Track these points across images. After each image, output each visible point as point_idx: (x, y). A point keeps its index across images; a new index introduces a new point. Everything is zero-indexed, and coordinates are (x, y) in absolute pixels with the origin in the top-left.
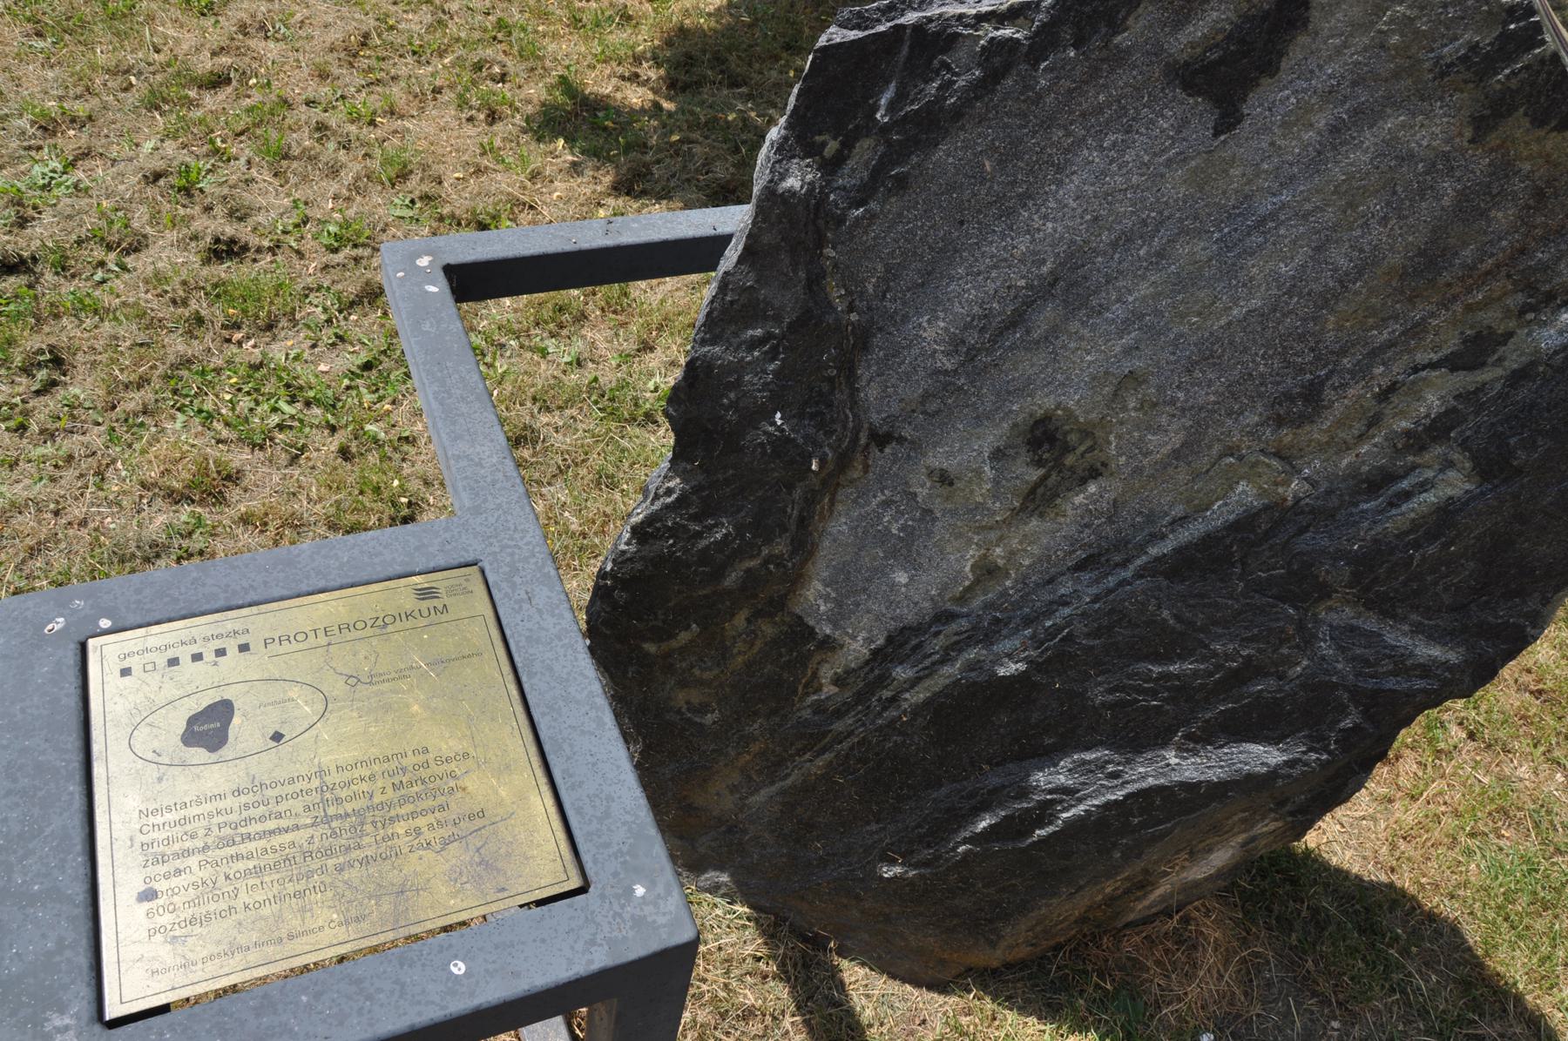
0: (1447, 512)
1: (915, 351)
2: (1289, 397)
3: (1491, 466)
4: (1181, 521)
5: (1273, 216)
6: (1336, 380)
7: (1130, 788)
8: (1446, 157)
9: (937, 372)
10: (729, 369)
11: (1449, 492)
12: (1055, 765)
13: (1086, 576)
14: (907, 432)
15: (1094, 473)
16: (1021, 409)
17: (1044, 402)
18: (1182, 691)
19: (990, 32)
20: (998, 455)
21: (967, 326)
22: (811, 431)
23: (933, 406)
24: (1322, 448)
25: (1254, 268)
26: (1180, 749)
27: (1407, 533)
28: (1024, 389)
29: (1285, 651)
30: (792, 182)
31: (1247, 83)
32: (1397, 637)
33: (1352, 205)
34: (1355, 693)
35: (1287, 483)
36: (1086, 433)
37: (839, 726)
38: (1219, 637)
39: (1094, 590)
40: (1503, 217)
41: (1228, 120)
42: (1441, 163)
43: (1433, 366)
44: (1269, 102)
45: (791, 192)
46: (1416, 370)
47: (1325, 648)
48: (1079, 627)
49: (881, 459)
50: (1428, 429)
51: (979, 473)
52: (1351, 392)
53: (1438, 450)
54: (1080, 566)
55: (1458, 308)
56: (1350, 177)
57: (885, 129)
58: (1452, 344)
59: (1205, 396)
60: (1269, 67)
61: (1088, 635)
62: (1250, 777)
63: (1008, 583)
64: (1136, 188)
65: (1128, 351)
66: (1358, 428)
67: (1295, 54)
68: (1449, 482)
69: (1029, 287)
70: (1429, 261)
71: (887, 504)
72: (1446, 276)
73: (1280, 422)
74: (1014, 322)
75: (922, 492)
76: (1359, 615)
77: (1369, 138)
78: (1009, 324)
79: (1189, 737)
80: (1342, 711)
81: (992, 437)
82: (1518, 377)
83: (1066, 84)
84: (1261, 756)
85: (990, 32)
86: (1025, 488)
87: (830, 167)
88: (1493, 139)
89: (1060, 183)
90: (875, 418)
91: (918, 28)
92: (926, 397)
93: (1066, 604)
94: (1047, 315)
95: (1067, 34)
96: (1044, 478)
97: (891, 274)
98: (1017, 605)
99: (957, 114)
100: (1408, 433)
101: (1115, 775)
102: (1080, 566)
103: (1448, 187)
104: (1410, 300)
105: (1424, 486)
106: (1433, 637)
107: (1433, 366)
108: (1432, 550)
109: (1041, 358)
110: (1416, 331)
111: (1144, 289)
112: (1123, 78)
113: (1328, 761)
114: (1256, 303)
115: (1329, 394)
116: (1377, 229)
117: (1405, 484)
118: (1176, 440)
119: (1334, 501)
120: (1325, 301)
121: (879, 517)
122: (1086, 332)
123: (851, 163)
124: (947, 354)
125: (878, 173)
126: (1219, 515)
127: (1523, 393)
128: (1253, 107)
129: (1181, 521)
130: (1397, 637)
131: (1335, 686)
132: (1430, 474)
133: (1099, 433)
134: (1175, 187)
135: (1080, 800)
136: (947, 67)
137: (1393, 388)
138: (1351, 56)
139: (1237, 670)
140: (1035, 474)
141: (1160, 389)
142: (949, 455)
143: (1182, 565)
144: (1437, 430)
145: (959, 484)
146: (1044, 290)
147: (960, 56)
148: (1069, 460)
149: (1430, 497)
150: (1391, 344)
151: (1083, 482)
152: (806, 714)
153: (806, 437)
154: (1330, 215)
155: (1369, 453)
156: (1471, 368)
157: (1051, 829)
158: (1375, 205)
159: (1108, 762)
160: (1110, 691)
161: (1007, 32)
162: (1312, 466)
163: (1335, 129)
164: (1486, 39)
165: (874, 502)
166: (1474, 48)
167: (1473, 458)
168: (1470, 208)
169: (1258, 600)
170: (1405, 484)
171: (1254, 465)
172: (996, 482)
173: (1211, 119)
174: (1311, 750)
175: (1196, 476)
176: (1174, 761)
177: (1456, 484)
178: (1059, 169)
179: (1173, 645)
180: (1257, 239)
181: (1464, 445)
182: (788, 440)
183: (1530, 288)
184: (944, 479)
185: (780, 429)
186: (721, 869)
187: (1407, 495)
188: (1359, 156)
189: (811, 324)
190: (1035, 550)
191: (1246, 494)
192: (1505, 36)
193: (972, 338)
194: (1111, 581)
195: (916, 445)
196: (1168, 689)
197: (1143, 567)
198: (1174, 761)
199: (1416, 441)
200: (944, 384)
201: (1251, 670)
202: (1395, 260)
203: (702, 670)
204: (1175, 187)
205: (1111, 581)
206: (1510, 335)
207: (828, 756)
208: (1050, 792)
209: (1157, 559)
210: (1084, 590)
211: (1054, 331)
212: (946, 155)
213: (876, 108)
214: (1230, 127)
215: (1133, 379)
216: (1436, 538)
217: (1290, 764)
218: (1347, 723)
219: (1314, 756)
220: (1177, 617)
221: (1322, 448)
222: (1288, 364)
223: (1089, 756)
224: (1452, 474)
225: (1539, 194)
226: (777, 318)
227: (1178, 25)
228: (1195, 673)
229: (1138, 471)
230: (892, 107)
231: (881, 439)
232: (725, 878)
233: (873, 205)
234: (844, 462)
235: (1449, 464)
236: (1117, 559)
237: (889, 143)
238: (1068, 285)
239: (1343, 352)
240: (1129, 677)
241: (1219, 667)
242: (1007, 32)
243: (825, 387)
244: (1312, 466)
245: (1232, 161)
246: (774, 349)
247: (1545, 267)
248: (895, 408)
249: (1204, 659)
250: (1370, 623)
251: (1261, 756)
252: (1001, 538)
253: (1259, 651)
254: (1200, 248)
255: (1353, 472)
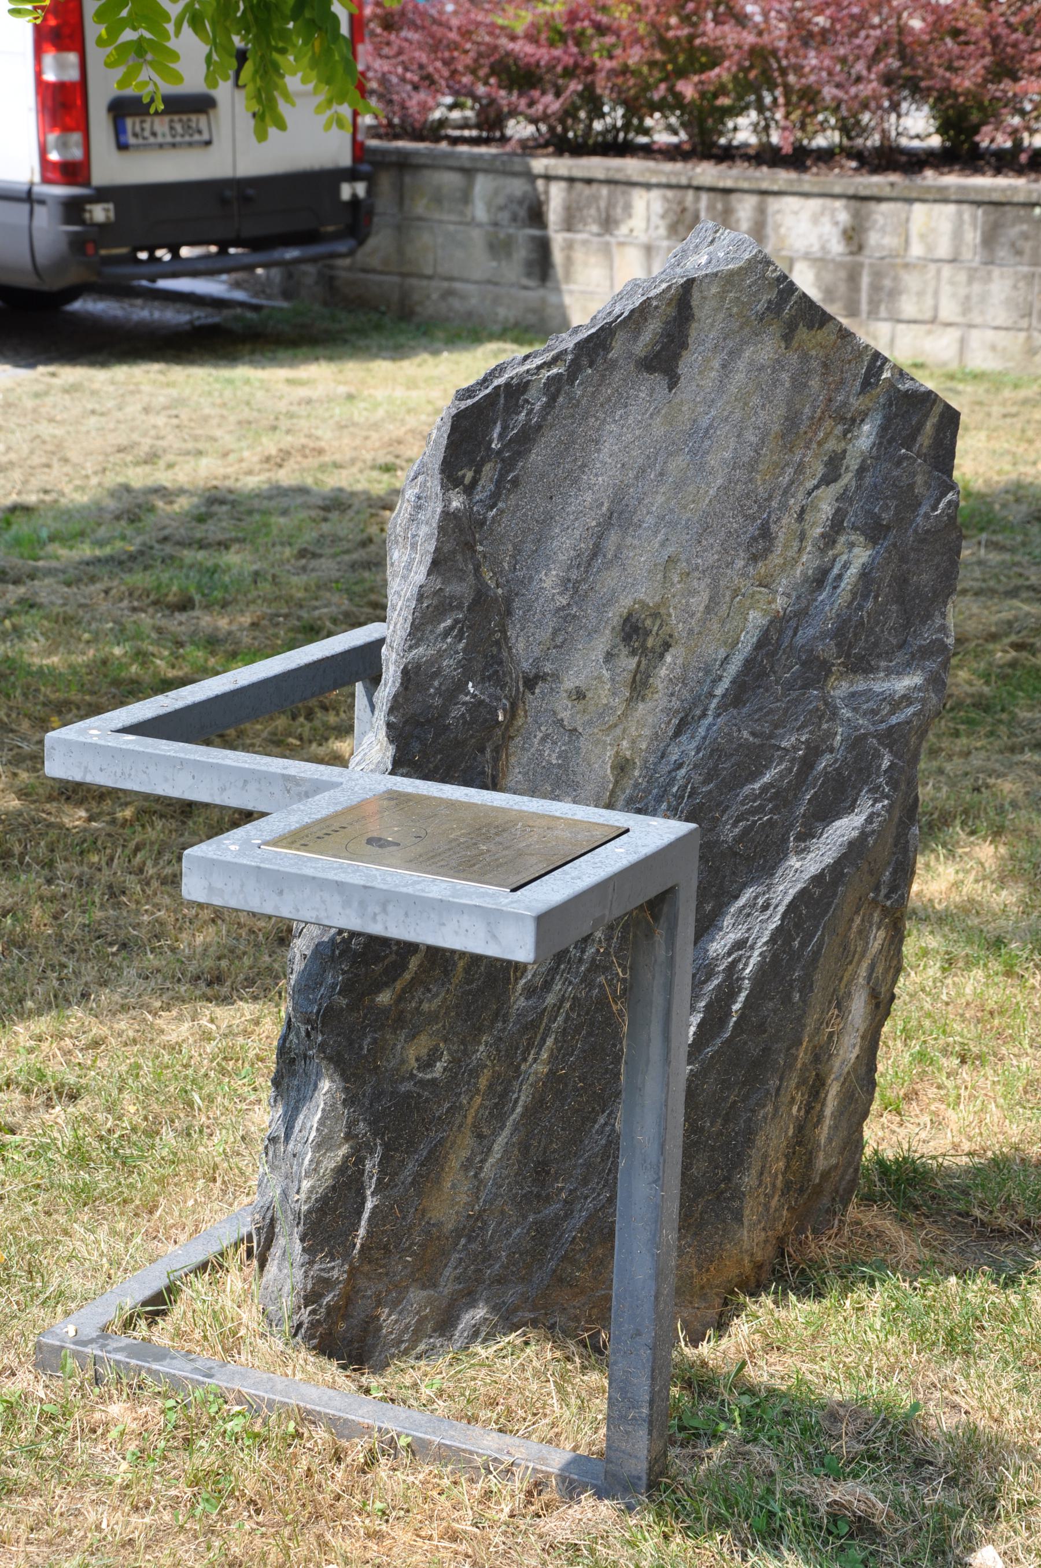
0: (865, 574)
1: (542, 600)
2: (754, 539)
3: (875, 532)
4: (726, 659)
5: (711, 426)
6: (774, 517)
7: (781, 909)
8: (778, 361)
9: (558, 610)
10: (431, 662)
11: (862, 560)
12: (721, 929)
13: (683, 738)
14: (548, 668)
15: (667, 646)
16: (614, 615)
17: (625, 603)
18: (781, 797)
19: (545, 374)
20: (609, 657)
21: (570, 568)
22: (492, 690)
23: (559, 640)
24: (783, 567)
25: (712, 461)
26: (799, 852)
27: (851, 603)
28: (611, 600)
29: (825, 726)
30: (455, 504)
31: (676, 357)
32: (880, 686)
33: (746, 404)
34: (880, 737)
35: (774, 600)
36: (655, 615)
37: (551, 999)
38: (783, 737)
39: (694, 744)
40: (815, 383)
41: (673, 382)
42: (778, 365)
43: (817, 487)
44: (689, 363)
45: (458, 509)
46: (809, 494)
47: (846, 713)
48: (697, 778)
49: (533, 701)
50: (832, 527)
51: (599, 678)
52: (784, 522)
53: (842, 539)
54: (677, 733)
55: (814, 446)
56: (740, 389)
57: (499, 452)
58: (820, 470)
59: (712, 557)
60: (684, 345)
61: (705, 783)
62: (851, 844)
63: (637, 773)
64: (638, 438)
65: (663, 545)
66: (796, 544)
67: (693, 333)
68: (857, 557)
69: (599, 525)
70: (792, 421)
71: (544, 740)
72: (803, 428)
73: (754, 558)
74: (594, 555)
75: (565, 715)
76: (852, 683)
77: (741, 365)
78: (592, 556)
79: (801, 838)
80: (878, 756)
81: (602, 643)
82: (861, 471)
83: (591, 389)
84: (845, 828)
85: (545, 374)
86: (629, 677)
87: (469, 490)
88: (795, 344)
89: (599, 451)
90: (525, 665)
91: (507, 385)
92: (555, 632)
93: (680, 766)
94: (613, 538)
95: (585, 361)
96: (639, 663)
97: (518, 550)
98: (647, 791)
99: (539, 427)
100: (823, 535)
101: (765, 907)
102: (677, 733)
103: (785, 376)
104: (791, 450)
105: (846, 566)
106: (899, 672)
107: (817, 487)
108: (869, 605)
109: (615, 572)
110: (800, 468)
111: (660, 499)
112: (618, 376)
113: (891, 806)
114: (720, 482)
115: (774, 528)
116: (762, 413)
117: (836, 571)
118: (705, 596)
119: (804, 603)
120: (752, 466)
121: (541, 753)
122: (636, 542)
123: (481, 483)
124: (561, 594)
125: (499, 483)
126: (748, 641)
127: (868, 481)
128: (682, 369)
129: (726, 659)
130: (880, 686)
131: (865, 737)
132: (845, 557)
133: (663, 611)
134: (659, 429)
135: (752, 948)
136: (527, 401)
137: (803, 511)
138: (719, 326)
139: (805, 755)
140: (633, 662)
141: (688, 561)
142: (578, 674)
143: (740, 693)
144: (836, 526)
145: (589, 695)
146: (607, 523)
147: (532, 394)
148: (650, 642)
149: (854, 570)
150: (792, 482)
151: (662, 656)
152: (522, 1002)
153: (490, 696)
154: (738, 415)
155: (808, 561)
156: (835, 480)
157: (742, 997)
158: (756, 400)
159: (756, 897)
160: (735, 825)
161: (555, 371)
162: (783, 584)
163: (724, 366)
164: (773, 295)
165: (536, 741)
166: (770, 302)
167: (863, 533)
168: (799, 385)
169: (794, 694)
170: (836, 571)
171: (753, 596)
172: (613, 680)
173: (665, 383)
174: (876, 801)
175: (723, 623)
176: (798, 865)
177: (861, 556)
178: (597, 442)
179: (755, 758)
180: (707, 443)
181: (855, 528)
182: (481, 702)
183: (842, 419)
184: (579, 695)
185: (474, 696)
186: (472, 1305)
187: (840, 577)
188: (739, 377)
189: (481, 599)
190: (647, 732)
191: (756, 619)
192: (780, 292)
193: (574, 575)
194: (702, 731)
195: (556, 677)
196: (770, 800)
197: (718, 708)
198: (798, 865)
199: (829, 539)
200: (566, 617)
201: (814, 752)
202: (776, 428)
203: (430, 1001)
204: (659, 429)
205: (702, 731)
206: (845, 451)
207: (550, 1042)
208: (729, 954)
209: (724, 696)
210: (687, 748)
211: (619, 548)
212: (537, 456)
213: (491, 442)
214: (676, 383)
215: (671, 560)
216: (868, 596)
217: (869, 820)
218: (886, 764)
219: (879, 805)
220: (753, 734)
221: (783, 567)
222: (746, 517)
223: (742, 901)
224: (856, 550)
225: (825, 365)
226: (459, 607)
227: (636, 338)
228: (782, 776)
229: (691, 631)
230: (501, 436)
231: (531, 683)
232: (480, 1312)
233: (500, 505)
234: (514, 706)
235: (852, 545)
236: (698, 712)
237: (503, 460)
238: (618, 516)
239: (770, 498)
240: (743, 803)
241: (793, 761)
242: (555, 371)
243: (495, 650)
244: (783, 584)
245: (681, 403)
246: (461, 630)
247: (845, 404)
248: (537, 652)
249: (781, 759)
250: (861, 686)
251: (845, 828)
252: (624, 731)
253: (811, 732)
254: (680, 461)
255: (806, 580)
